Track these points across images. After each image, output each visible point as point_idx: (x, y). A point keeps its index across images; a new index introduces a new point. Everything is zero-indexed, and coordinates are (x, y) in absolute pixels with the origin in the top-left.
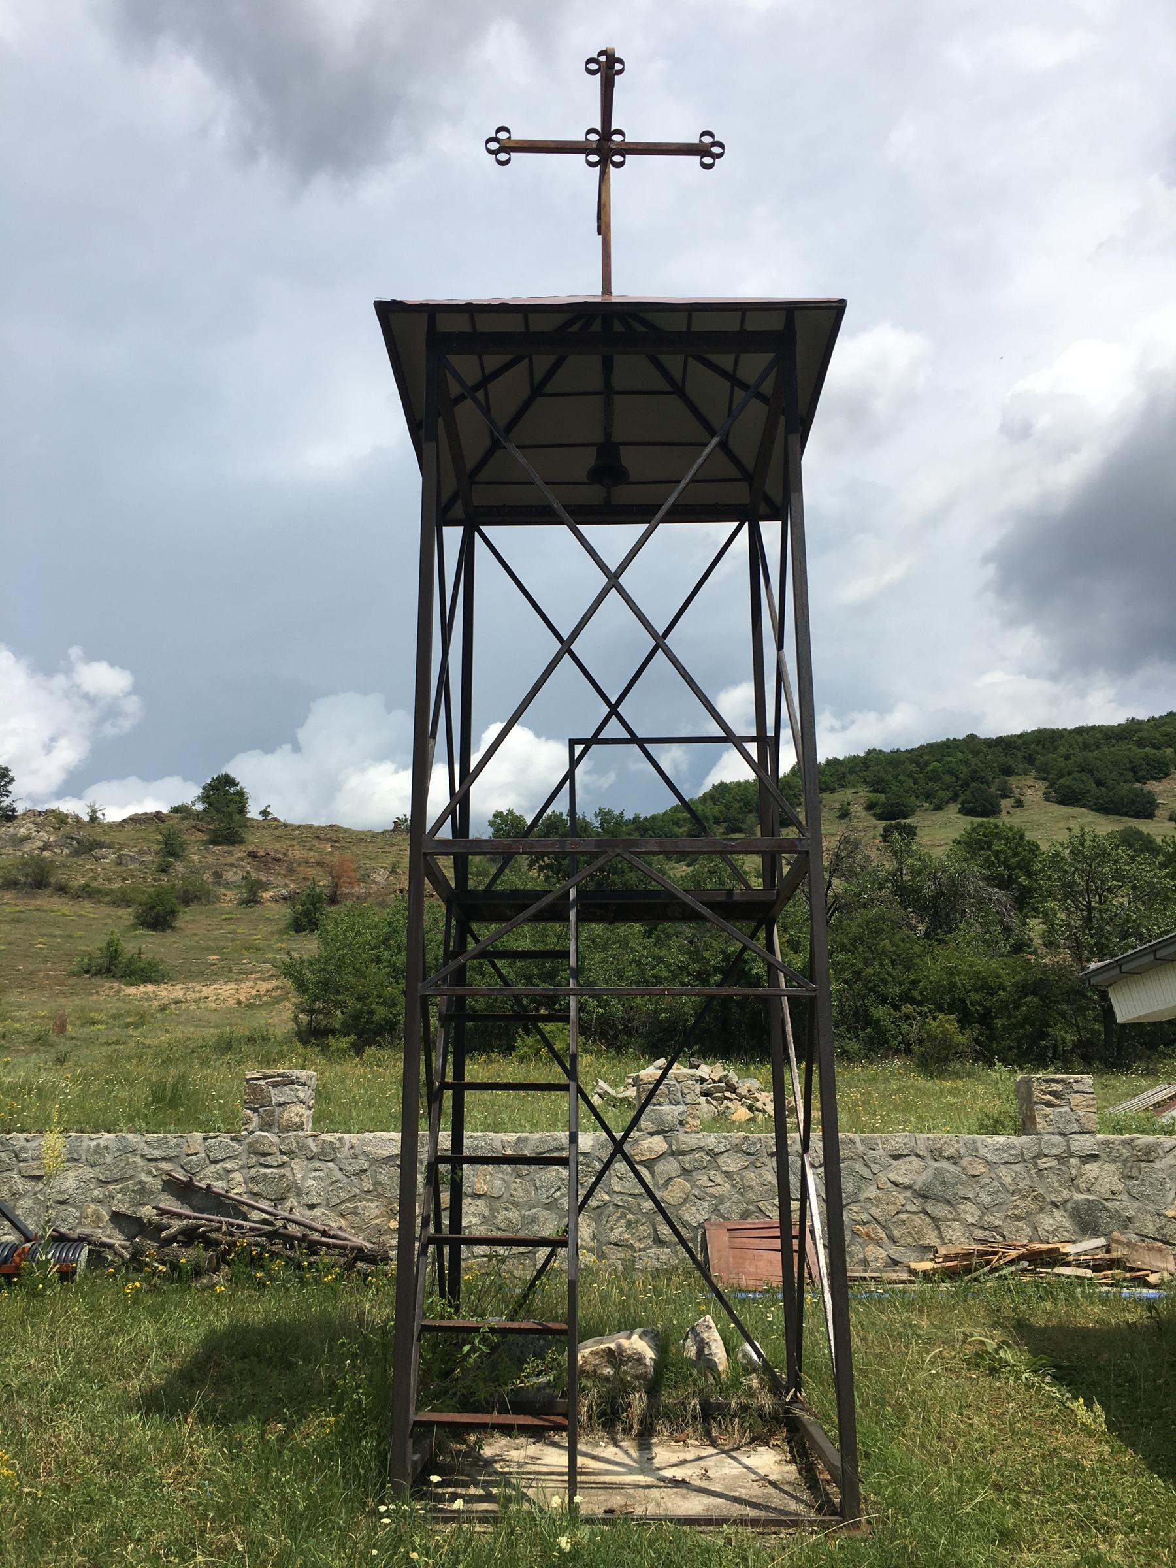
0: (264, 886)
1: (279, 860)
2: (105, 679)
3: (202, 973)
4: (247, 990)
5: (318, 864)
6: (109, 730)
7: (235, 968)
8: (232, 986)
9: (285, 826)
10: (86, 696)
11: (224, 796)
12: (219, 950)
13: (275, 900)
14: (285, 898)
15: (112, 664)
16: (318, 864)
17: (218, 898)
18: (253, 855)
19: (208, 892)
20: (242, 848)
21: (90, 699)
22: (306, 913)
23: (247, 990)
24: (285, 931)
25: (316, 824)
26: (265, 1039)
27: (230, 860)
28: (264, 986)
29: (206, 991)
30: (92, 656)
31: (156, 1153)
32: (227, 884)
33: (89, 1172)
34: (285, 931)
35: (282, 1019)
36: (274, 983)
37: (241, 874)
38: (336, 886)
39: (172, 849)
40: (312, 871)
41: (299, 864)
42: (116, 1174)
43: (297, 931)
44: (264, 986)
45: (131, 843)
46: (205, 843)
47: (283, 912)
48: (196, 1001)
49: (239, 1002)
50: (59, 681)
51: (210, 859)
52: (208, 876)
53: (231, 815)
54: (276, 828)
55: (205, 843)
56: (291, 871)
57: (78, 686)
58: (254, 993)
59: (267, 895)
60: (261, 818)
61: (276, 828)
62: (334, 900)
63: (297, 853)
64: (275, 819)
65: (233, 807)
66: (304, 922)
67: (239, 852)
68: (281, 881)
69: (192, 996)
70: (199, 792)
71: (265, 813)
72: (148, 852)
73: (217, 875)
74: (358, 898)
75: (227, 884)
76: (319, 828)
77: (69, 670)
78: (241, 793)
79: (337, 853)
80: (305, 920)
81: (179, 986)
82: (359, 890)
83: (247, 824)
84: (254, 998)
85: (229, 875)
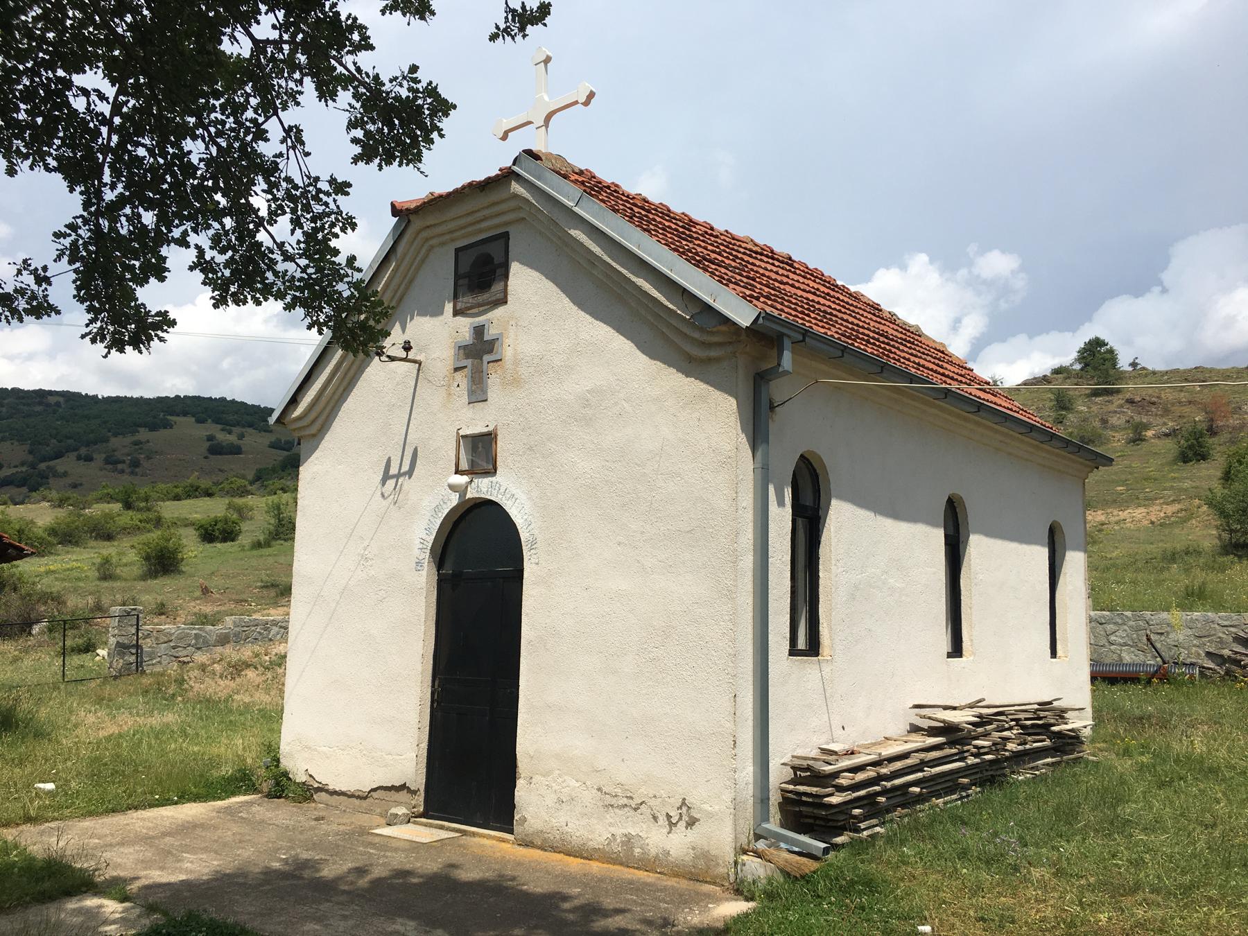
0: (1146, 427)
1: (1154, 403)
2: (998, 264)
3: (1115, 501)
4: (1157, 512)
5: (1190, 402)
6: (1003, 305)
7: (1141, 496)
8: (1142, 510)
9: (1154, 373)
10: (985, 282)
11: (1096, 356)
12: (1124, 483)
13: (1157, 437)
14: (1167, 435)
15: (1003, 252)
16: (1190, 402)
17: (1108, 440)
18: (1131, 402)
19: (1100, 436)
20: (1120, 396)
21: (989, 284)
22: (1190, 447)
23: (1157, 512)
24: (1174, 462)
25: (1182, 368)
26: (1199, 553)
27: (1112, 408)
28: (1170, 509)
29: (1123, 515)
30: (984, 250)
31: (1226, 623)
32: (1113, 428)
33: (1190, 632)
34: (1174, 462)
35: (1204, 532)
36: (1177, 507)
37: (1123, 419)
38: (1212, 420)
39: (1063, 404)
40: (1187, 410)
41: (1173, 404)
42: (1204, 633)
43: (1185, 462)
44: (1170, 509)
45: (1029, 403)
46: (1088, 396)
47: (1170, 447)
48: (1117, 523)
49: (1152, 523)
50: (963, 272)
51: (1095, 408)
52: (1097, 424)
53: (1107, 371)
54: (1146, 376)
55: (1088, 396)
56: (1167, 411)
57: (978, 276)
58: (1162, 515)
59: (1150, 433)
60: (1130, 369)
61: (1146, 376)
62: (1212, 432)
63: (1169, 396)
64: (1144, 368)
65: (1108, 364)
66: (1190, 454)
67: (1117, 400)
68: (1160, 421)
69: (1113, 519)
70: (1075, 355)
71: (1134, 364)
72: (1044, 408)
73: (1104, 421)
74: (1234, 428)
75: (1113, 428)
76: (1185, 371)
77: (970, 264)
78: (1111, 351)
79: (1206, 391)
80: (1193, 451)
81: (1100, 512)
82: (1234, 421)
83: (1121, 377)
84: (1164, 518)
85: (1114, 420)
